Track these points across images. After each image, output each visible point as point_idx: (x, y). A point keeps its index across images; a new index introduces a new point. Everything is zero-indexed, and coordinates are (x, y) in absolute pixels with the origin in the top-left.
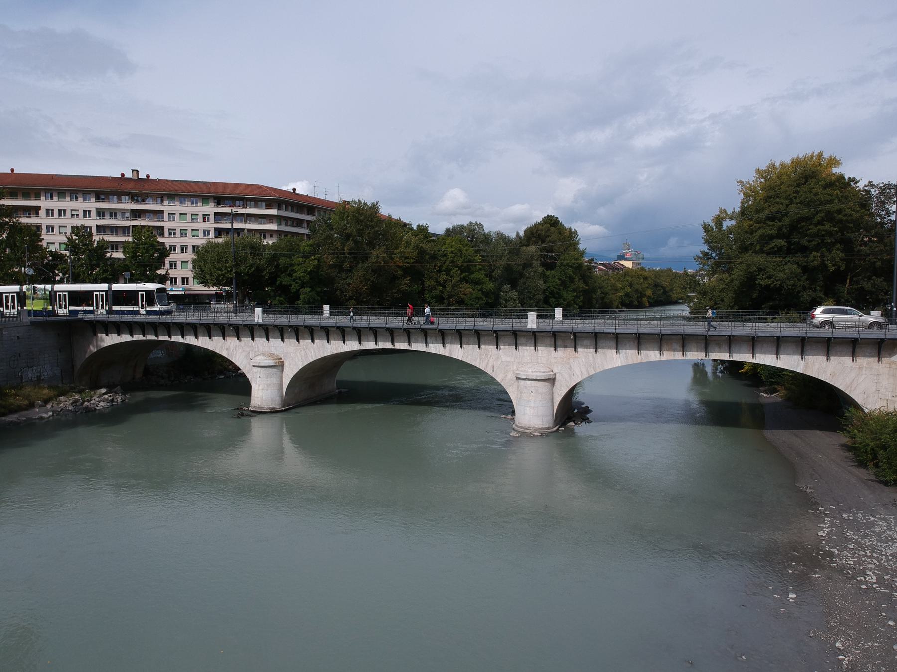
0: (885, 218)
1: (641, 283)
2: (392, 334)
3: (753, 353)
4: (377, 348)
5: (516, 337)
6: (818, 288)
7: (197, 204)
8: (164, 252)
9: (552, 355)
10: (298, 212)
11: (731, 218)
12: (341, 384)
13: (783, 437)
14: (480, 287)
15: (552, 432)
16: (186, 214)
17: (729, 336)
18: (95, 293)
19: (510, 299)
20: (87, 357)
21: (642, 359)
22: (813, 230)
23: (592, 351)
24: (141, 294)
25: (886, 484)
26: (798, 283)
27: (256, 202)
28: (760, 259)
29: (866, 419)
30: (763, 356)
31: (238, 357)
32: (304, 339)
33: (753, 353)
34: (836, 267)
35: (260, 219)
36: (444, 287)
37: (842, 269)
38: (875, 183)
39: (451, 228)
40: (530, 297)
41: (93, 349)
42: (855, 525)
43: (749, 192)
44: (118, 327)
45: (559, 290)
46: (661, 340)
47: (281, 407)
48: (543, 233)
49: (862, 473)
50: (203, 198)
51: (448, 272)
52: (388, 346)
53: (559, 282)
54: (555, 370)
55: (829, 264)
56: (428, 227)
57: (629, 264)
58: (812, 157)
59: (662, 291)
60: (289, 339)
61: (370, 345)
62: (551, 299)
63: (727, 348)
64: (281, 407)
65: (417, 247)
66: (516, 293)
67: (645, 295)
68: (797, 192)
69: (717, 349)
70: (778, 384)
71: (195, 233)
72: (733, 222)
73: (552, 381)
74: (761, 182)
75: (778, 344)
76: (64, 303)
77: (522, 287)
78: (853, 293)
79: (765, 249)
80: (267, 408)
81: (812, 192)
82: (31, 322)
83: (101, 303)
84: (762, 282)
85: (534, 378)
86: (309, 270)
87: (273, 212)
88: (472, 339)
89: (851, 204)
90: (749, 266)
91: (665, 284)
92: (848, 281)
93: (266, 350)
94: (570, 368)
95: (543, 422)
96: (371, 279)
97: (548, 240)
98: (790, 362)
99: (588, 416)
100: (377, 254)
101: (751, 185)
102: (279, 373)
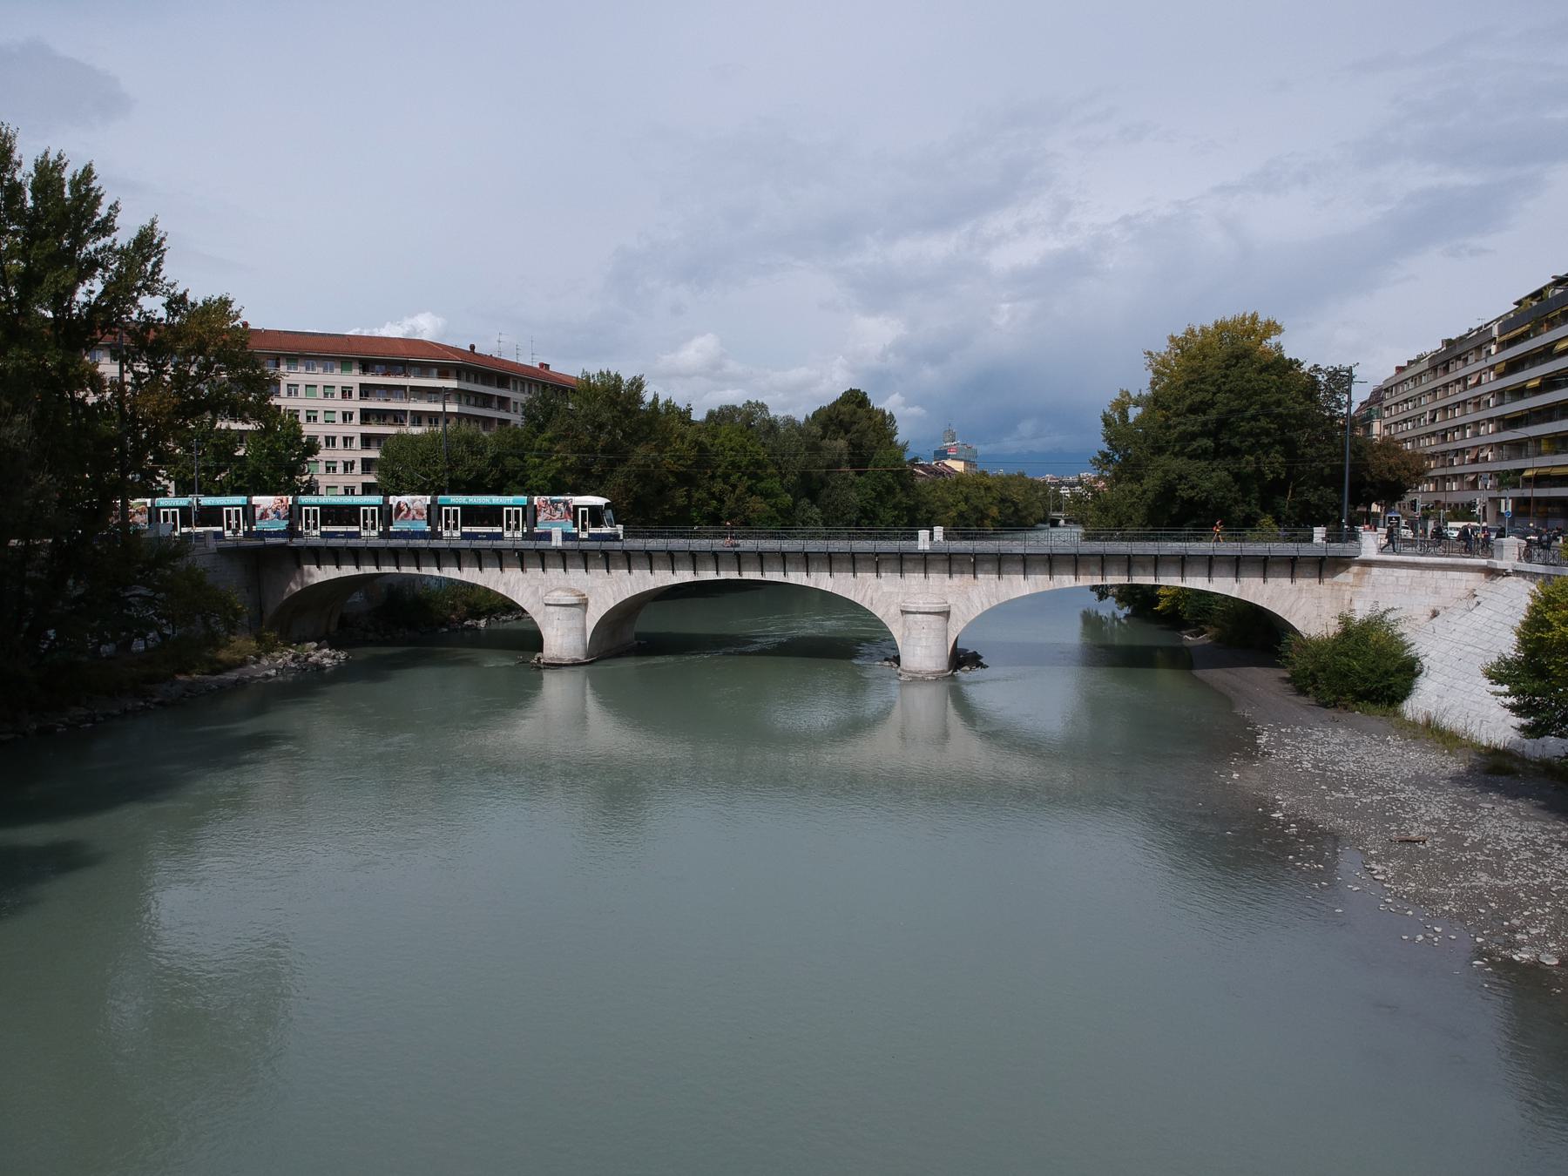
0: (1336, 411)
1: (982, 497)
2: (739, 559)
3: (1182, 576)
4: (718, 578)
5: (902, 562)
6: (1253, 501)
7: (332, 370)
8: (312, 448)
9: (946, 583)
10: (484, 383)
11: (1137, 404)
12: (638, 636)
13: (1218, 676)
14: (774, 501)
15: (946, 677)
16: (316, 386)
17: (1156, 556)
18: (362, 508)
19: (809, 520)
20: (285, 597)
21: (1054, 585)
22: (1245, 427)
23: (995, 576)
24: (164, 512)
25: (1325, 706)
26: (1229, 495)
27: (424, 369)
28: (1179, 464)
29: (1305, 644)
30: (1193, 579)
31: (521, 594)
32: (616, 568)
33: (1182, 576)
34: (1275, 475)
35: (429, 395)
36: (721, 501)
37: (1282, 477)
38: (1323, 367)
39: (717, 410)
40: (837, 518)
41: (295, 587)
42: (1293, 735)
43: (1160, 369)
44: (336, 556)
45: (875, 506)
46: (1076, 561)
47: (586, 659)
48: (847, 418)
49: (1303, 700)
50: (342, 362)
51: (726, 478)
52: (734, 575)
53: (874, 494)
54: (950, 601)
55: (1266, 469)
56: (691, 409)
57: (958, 466)
58: (1244, 320)
59: (1013, 508)
60: (595, 568)
61: (709, 575)
62: (863, 521)
63: (1153, 571)
64: (586, 659)
65: (696, 442)
66: (818, 510)
67: (988, 516)
68: (1226, 376)
69: (1141, 572)
70: (1206, 623)
71: (329, 417)
72: (1139, 410)
73: (946, 614)
74: (1176, 355)
75: (1210, 564)
76: (235, 522)
77: (825, 501)
78: (1296, 507)
79: (1186, 450)
80: (569, 660)
81: (1243, 377)
82: (218, 549)
83: (235, 522)
84: (1184, 494)
85: (927, 610)
86: (550, 475)
87: (452, 384)
88: (845, 565)
89: (1294, 393)
90: (1166, 472)
91: (1017, 498)
92: (1290, 492)
93: (562, 583)
94: (969, 599)
95: (937, 664)
96: (635, 489)
97: (855, 428)
98: (1223, 585)
99: (981, 661)
100: (641, 453)
101: (1163, 358)
102: (582, 613)
